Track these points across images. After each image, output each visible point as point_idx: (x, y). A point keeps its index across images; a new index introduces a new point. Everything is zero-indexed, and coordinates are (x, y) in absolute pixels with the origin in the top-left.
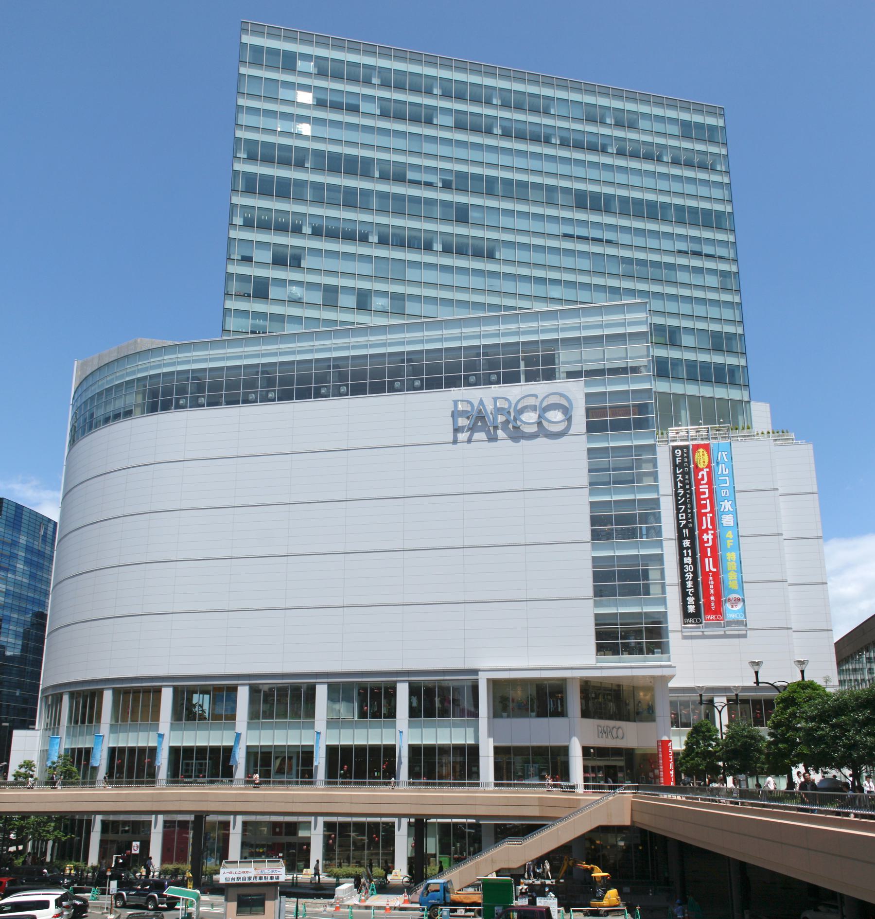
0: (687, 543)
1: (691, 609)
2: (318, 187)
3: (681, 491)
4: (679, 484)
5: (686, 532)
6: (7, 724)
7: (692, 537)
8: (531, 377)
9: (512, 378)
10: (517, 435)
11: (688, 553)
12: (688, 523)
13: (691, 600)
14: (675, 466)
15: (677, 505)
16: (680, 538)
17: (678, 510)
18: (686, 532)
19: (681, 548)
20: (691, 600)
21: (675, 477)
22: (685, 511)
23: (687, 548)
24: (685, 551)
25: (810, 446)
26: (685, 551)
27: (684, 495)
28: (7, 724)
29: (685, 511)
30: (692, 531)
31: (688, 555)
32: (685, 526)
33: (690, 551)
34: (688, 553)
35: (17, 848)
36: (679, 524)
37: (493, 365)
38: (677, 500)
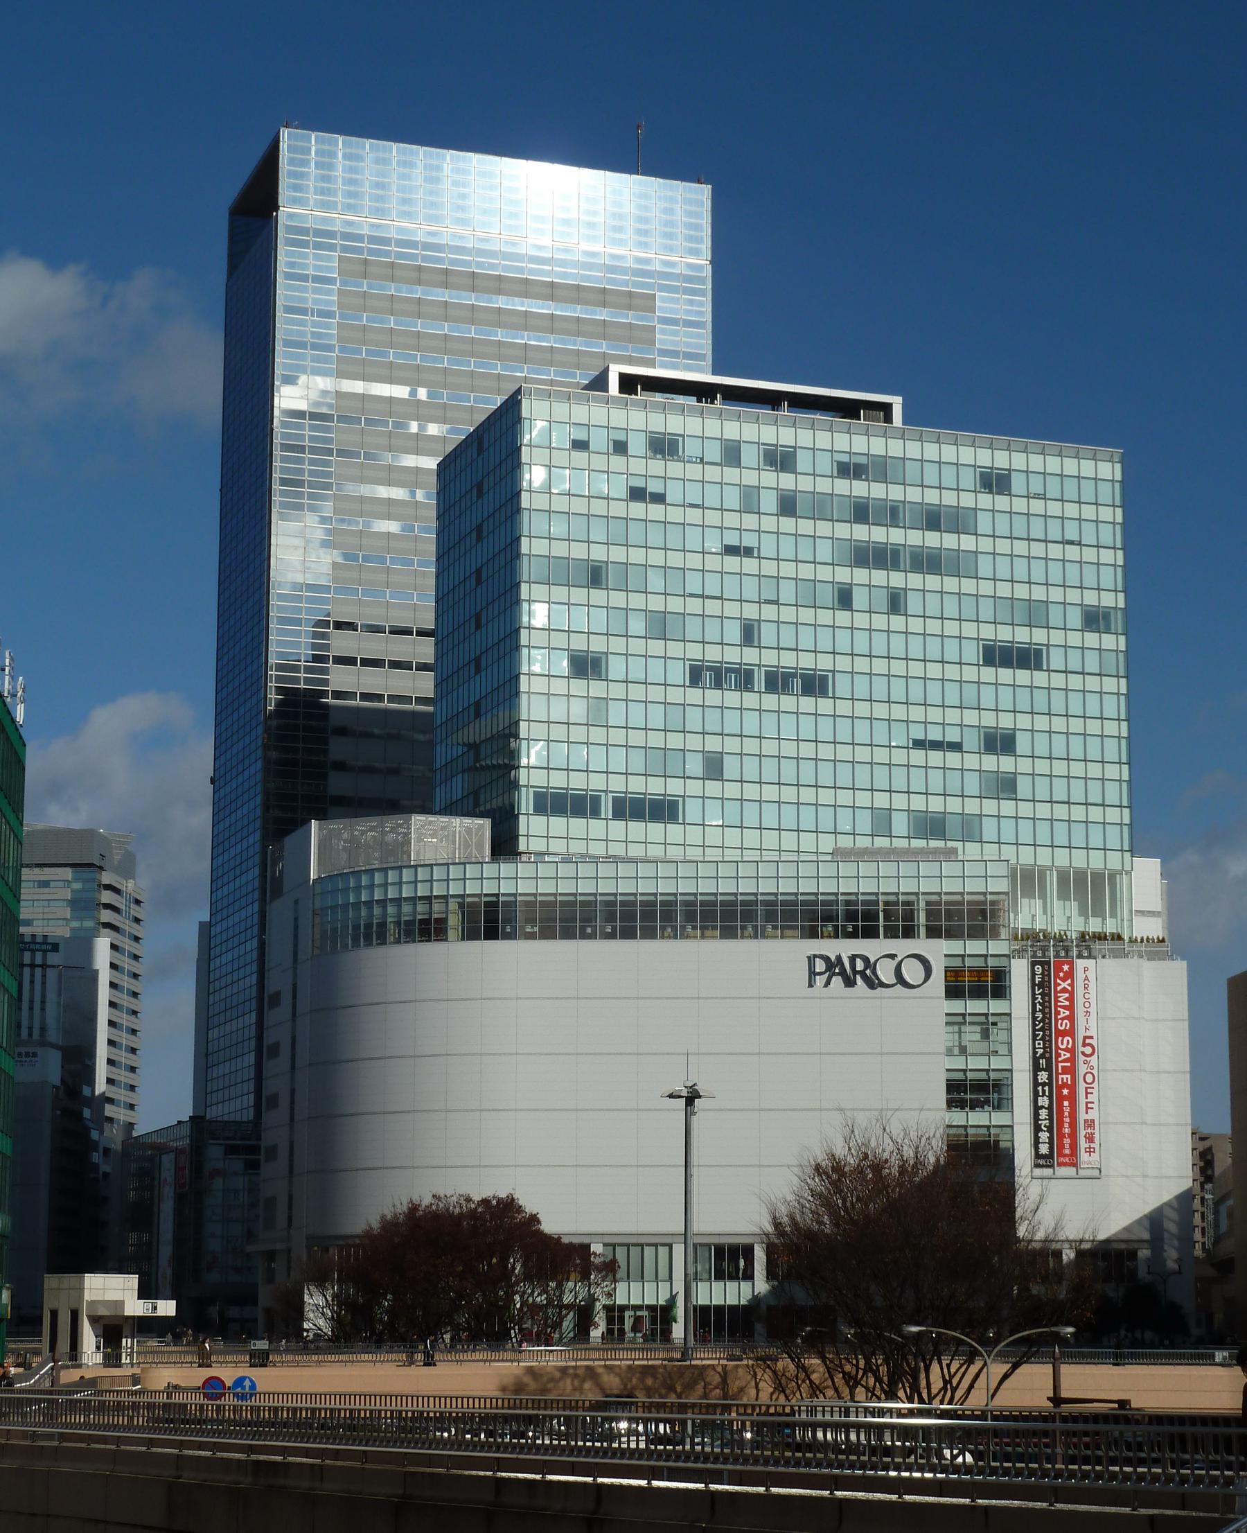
0: (1043, 1077)
1: (1044, 1149)
2: (669, 1468)
3: (1040, 1015)
4: (1038, 1006)
5: (1043, 1062)
6: (393, 527)
7: (1048, 1069)
8: (891, 933)
9: (871, 933)
10: (873, 983)
11: (1044, 1091)
12: (1045, 1052)
13: (1044, 1136)
14: (1033, 985)
15: (1034, 1030)
16: (1036, 1068)
17: (1034, 1037)
18: (1043, 1062)
19: (1036, 1084)
20: (1044, 1136)
21: (1034, 998)
22: (1043, 1039)
23: (1044, 1084)
24: (1040, 1088)
25: (1185, 963)
26: (1040, 1088)
27: (1042, 1020)
28: (393, 527)
29: (1043, 1039)
30: (1049, 1061)
31: (1044, 1094)
32: (1042, 1056)
33: (1047, 1088)
34: (1044, 1091)
35: (421, 428)
36: (1035, 1053)
37: (851, 916)
38: (1034, 1025)
